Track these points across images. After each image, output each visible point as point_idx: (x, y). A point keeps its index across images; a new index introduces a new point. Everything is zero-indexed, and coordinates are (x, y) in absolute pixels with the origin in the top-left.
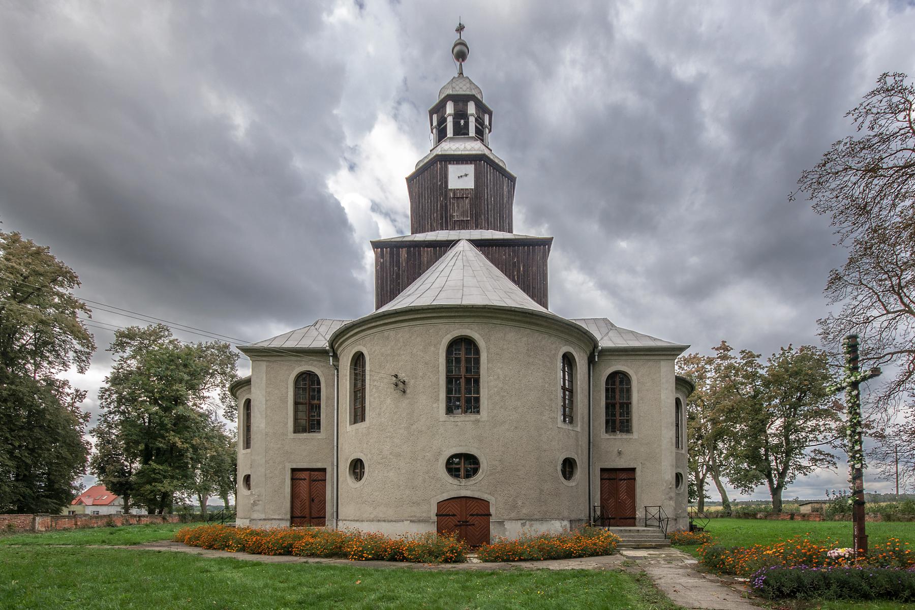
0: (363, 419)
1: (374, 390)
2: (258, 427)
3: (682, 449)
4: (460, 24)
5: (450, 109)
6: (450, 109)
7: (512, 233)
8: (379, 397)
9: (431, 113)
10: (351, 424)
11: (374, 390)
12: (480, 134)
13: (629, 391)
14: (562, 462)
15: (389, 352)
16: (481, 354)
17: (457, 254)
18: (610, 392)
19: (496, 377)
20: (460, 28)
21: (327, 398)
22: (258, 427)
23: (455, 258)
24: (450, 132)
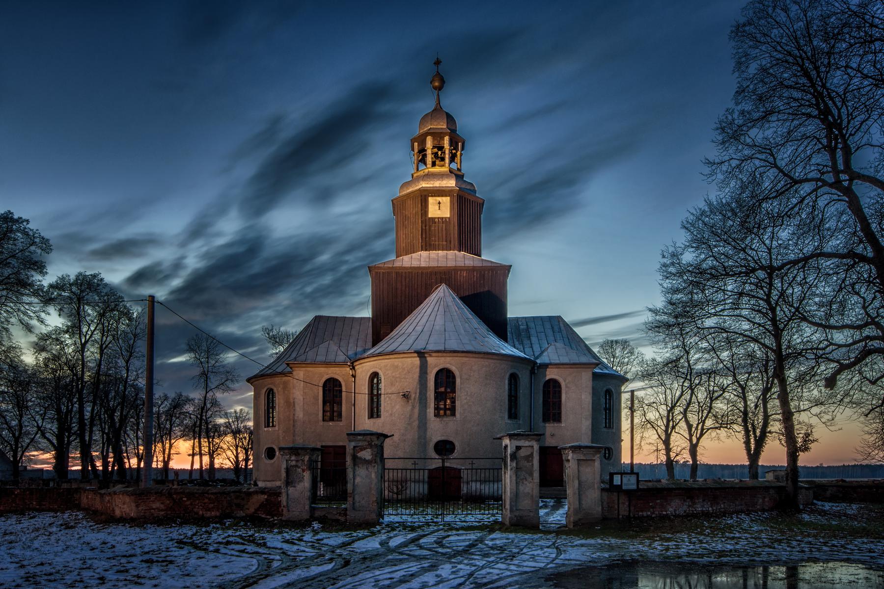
0: (378, 416)
1: (387, 399)
2: (298, 417)
3: (613, 428)
4: (438, 59)
5: (429, 143)
6: (429, 143)
7: (480, 256)
8: (391, 404)
9: (413, 141)
10: (368, 418)
11: (387, 399)
12: (453, 158)
13: (560, 392)
14: (182, 468)
15: (398, 376)
16: (457, 379)
17: (440, 300)
18: (546, 393)
19: (466, 393)
20: (438, 63)
21: (347, 397)
22: (298, 417)
23: (438, 304)
24: (429, 159)
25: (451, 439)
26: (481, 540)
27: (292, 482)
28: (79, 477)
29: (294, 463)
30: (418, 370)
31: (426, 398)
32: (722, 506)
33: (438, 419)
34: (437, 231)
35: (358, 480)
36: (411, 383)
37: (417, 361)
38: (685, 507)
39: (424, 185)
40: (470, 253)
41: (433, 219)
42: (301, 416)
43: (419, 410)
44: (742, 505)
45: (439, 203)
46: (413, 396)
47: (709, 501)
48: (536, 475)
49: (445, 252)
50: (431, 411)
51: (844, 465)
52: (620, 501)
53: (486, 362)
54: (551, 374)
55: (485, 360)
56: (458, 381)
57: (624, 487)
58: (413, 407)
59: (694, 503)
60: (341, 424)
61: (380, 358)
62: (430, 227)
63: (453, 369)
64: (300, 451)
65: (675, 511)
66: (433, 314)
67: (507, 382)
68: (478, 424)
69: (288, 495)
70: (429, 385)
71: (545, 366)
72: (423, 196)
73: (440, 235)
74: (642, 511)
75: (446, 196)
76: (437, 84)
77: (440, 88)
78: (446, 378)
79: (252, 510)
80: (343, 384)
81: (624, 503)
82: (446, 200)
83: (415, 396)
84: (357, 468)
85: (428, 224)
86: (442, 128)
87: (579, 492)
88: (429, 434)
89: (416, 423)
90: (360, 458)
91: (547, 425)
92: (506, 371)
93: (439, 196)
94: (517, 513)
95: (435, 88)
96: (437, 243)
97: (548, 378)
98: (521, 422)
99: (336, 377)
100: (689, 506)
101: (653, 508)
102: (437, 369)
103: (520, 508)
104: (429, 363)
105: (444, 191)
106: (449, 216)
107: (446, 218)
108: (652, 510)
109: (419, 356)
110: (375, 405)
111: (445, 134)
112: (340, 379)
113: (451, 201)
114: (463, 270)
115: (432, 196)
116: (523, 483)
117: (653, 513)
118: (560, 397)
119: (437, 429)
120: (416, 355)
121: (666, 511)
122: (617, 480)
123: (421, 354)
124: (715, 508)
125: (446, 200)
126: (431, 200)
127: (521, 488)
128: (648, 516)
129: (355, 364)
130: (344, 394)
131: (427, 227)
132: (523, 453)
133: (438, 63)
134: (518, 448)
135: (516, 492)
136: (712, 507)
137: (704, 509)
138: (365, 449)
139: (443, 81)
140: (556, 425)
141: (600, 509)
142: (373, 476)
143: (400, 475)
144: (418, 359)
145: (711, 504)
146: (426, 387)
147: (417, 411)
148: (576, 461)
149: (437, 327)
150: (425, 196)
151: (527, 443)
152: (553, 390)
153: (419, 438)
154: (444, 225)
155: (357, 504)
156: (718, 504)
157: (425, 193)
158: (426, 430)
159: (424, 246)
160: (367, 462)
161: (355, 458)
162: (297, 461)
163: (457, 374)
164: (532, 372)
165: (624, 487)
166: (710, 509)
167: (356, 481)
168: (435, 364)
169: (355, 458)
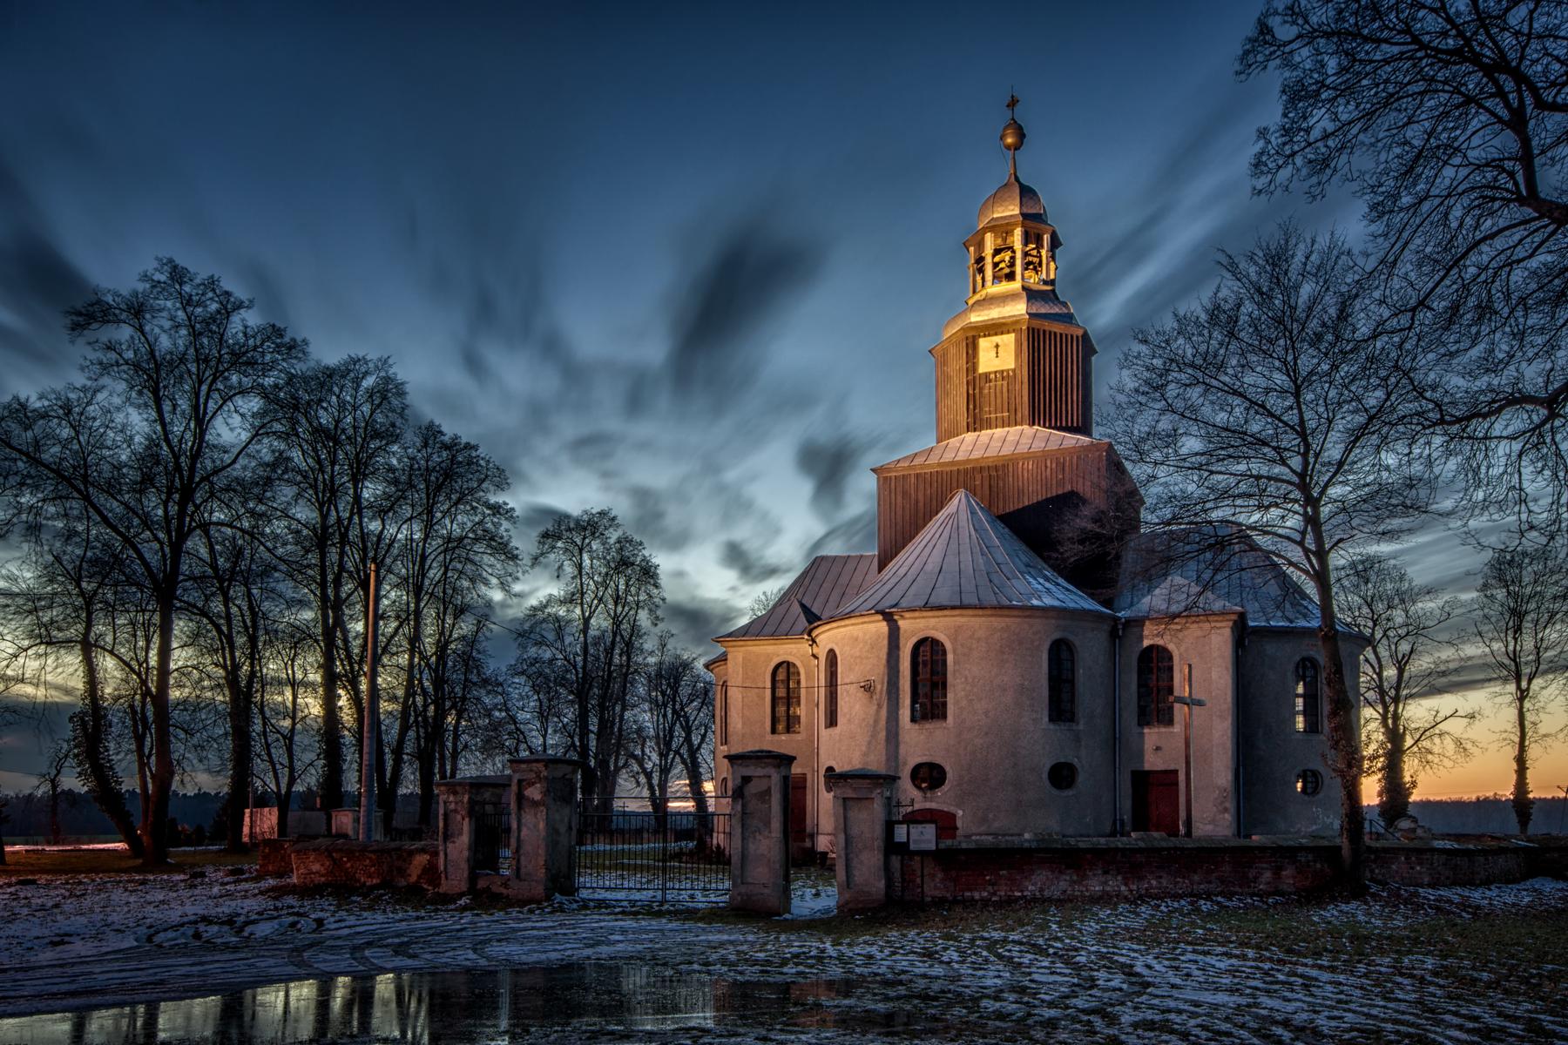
10: (913, 720)
25: (938, 761)
26: (298, 922)
27: (452, 836)
28: (686, 824)
29: (452, 806)
30: (886, 642)
31: (898, 689)
32: (1154, 882)
33: (917, 726)
34: (993, 395)
35: (524, 832)
36: (874, 667)
37: (883, 627)
38: (1063, 885)
39: (976, 317)
40: (1050, 427)
41: (987, 375)
42: (740, 726)
43: (888, 712)
44: (1210, 882)
45: (997, 346)
46: (879, 687)
47: (1119, 873)
48: (776, 824)
49: (1007, 429)
50: (905, 713)
51: (1478, 799)
52: (925, 872)
53: (998, 622)
54: (1150, 637)
55: (999, 619)
56: (950, 658)
57: (912, 847)
58: (879, 706)
59: (1084, 877)
60: (798, 737)
61: (834, 625)
62: (981, 389)
63: (941, 637)
64: (458, 789)
65: (1041, 890)
66: (931, 545)
67: (1045, 656)
68: (987, 734)
69: (446, 855)
70: (901, 668)
71: (1139, 622)
72: (971, 340)
73: (999, 401)
74: (971, 890)
75: (1008, 332)
76: (1009, 140)
77: (1017, 147)
78: (929, 656)
79: (413, 878)
80: (802, 671)
81: (933, 876)
82: (1008, 340)
83: (881, 688)
84: (523, 815)
85: (975, 382)
86: (1005, 218)
87: (847, 855)
88: (902, 750)
89: (883, 735)
90: (528, 799)
91: (1146, 730)
92: (1043, 635)
93: (996, 334)
94: (743, 889)
95: (1008, 147)
96: (993, 416)
97: (1146, 643)
98: (1081, 727)
99: (791, 659)
100: (1073, 882)
101: (993, 885)
102: (914, 640)
103: (750, 880)
104: (902, 631)
105: (1004, 324)
106: (1013, 367)
107: (1008, 371)
108: (990, 888)
109: (884, 619)
110: (1455, 678)
111: (1015, 225)
112: (798, 664)
113: (1018, 343)
114: (1028, 458)
115: (985, 336)
116: (755, 838)
117: (994, 894)
118: (1171, 678)
119: (919, 744)
120: (881, 617)
121: (1022, 891)
122: (901, 833)
123: (888, 617)
124: (1135, 887)
125: (1008, 340)
126: (985, 344)
127: (752, 847)
128: (982, 899)
129: (814, 635)
130: (803, 692)
131: (977, 391)
132: (752, 788)
133: (1013, 103)
134: (746, 780)
135: (742, 852)
136: (1126, 885)
137: (1108, 889)
138: (533, 784)
139: (1021, 136)
140: (1163, 730)
141: (882, 884)
142: (542, 825)
143: (685, 821)
144: (885, 623)
145: (1124, 878)
146: (898, 672)
147: (884, 712)
148: (841, 801)
149: (929, 567)
150: (974, 337)
151: (760, 772)
152: (1156, 663)
153: (888, 760)
154: (1005, 383)
155: (523, 870)
156: (1141, 879)
157: (970, 334)
158: (897, 746)
159: (971, 425)
160: (535, 804)
161: (520, 797)
162: (456, 803)
163: (948, 646)
164: (1114, 635)
165: (912, 847)
166: (1123, 888)
167: (522, 834)
168: (913, 627)
169: (520, 797)
